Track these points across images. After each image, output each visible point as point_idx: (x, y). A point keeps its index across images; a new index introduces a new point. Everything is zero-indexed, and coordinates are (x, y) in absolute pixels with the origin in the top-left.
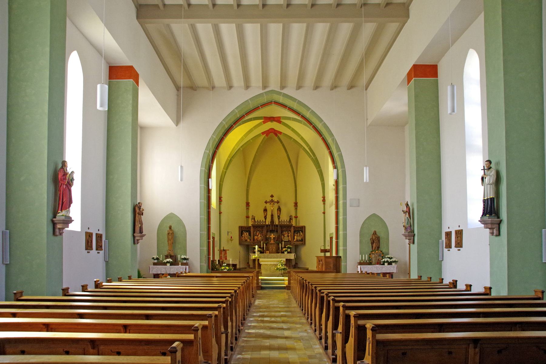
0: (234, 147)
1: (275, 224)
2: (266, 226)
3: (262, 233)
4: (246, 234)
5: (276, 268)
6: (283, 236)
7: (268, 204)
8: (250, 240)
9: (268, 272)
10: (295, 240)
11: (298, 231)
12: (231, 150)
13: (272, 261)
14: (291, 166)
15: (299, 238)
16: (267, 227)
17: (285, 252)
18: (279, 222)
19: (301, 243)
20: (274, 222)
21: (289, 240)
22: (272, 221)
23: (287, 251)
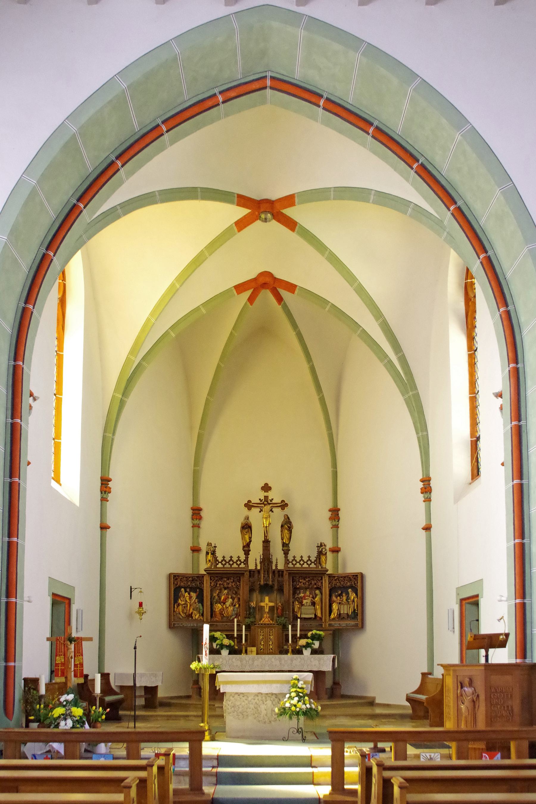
0: (148, 320)
1: (274, 568)
2: (247, 574)
3: (236, 593)
4: (190, 598)
5: (276, 710)
6: (297, 605)
7: (255, 511)
8: (203, 615)
9: (249, 723)
10: (332, 616)
11: (344, 589)
12: (139, 329)
13: (265, 682)
14: (322, 401)
15: (346, 610)
16: (250, 576)
17: (305, 651)
18: (287, 561)
19: (352, 623)
20: (272, 562)
21: (315, 615)
22: (266, 559)
23: (311, 647)
